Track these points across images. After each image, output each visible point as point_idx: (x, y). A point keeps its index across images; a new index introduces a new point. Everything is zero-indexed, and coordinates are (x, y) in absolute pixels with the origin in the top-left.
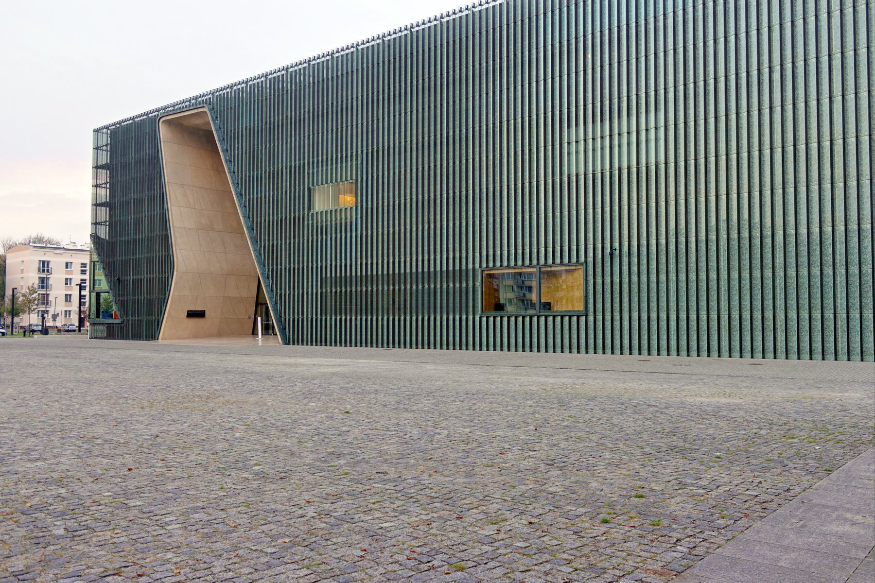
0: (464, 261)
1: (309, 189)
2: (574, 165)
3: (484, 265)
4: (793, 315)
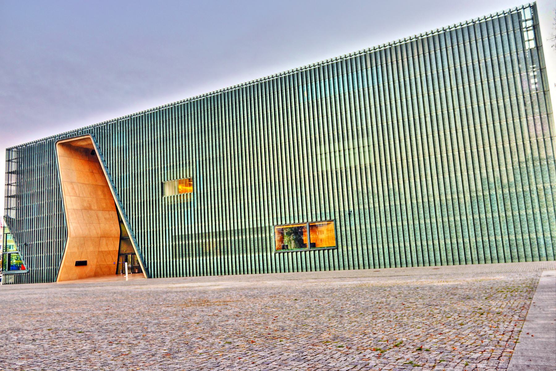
0: (259, 222)
1: (162, 184)
2: (323, 166)
3: (275, 223)
4: (350, 248)
